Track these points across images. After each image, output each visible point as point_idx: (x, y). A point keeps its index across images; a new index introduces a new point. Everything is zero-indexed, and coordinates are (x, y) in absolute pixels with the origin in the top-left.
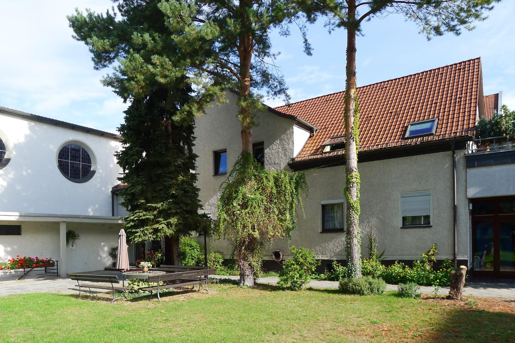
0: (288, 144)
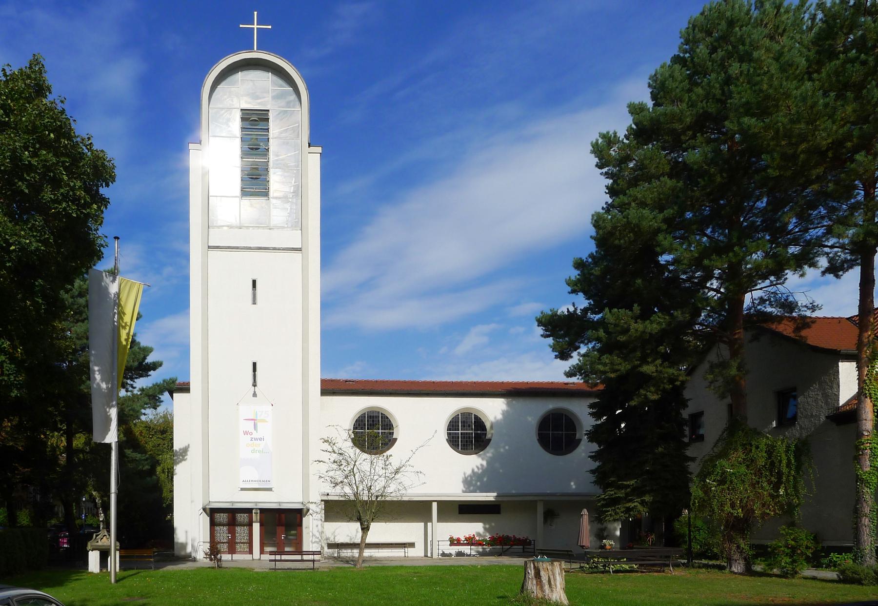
0: (831, 389)
